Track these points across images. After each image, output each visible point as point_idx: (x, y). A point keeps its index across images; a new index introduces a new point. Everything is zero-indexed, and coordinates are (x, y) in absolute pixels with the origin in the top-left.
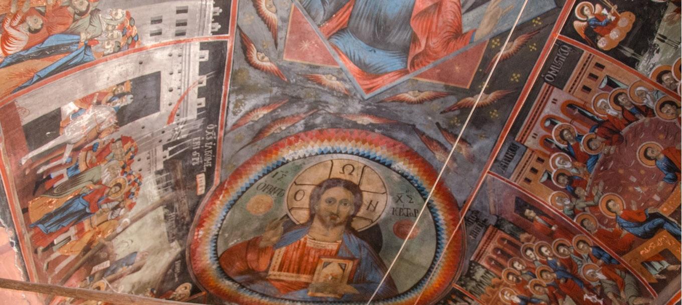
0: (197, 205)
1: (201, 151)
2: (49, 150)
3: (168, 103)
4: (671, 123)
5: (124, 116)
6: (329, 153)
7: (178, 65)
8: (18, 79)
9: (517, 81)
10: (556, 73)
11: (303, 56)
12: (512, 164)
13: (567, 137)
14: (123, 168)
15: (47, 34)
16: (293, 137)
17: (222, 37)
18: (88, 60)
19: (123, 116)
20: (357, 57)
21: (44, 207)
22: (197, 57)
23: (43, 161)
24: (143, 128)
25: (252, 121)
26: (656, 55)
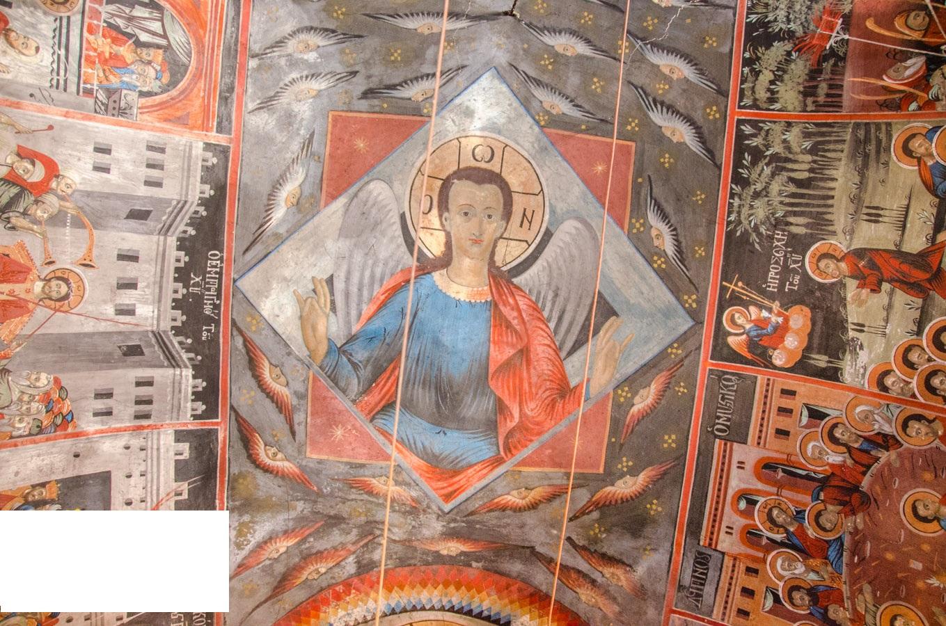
4: (931, 448)
6: (404, 611)
7: (139, 464)
9: (674, 445)
10: (729, 420)
11: (336, 449)
12: (709, 589)
13: (780, 520)
16: (341, 586)
17: (208, 424)
20: (419, 445)
22: (172, 453)
25: (270, 559)
26: (861, 353)
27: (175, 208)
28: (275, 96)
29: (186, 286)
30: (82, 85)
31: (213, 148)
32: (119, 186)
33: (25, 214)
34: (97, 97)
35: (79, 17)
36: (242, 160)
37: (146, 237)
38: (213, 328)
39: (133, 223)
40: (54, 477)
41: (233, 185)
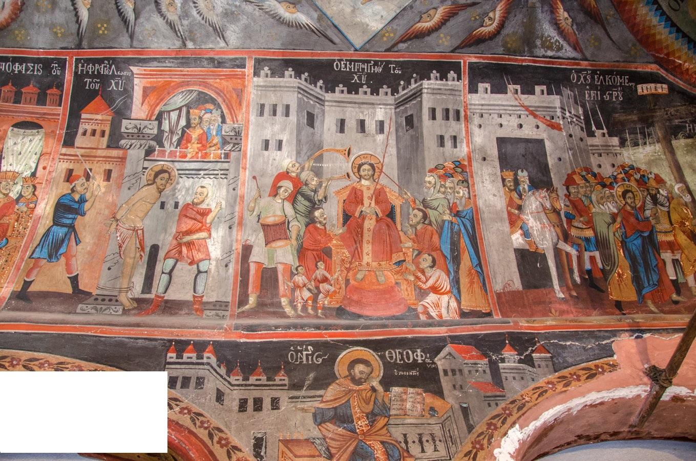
0: (683, 94)
1: (604, 89)
2: (557, 268)
3: (535, 129)
5: (541, 181)
8: (475, 285)
14: (604, 186)
15: (438, 252)
17: (465, 69)
18: (471, 214)
19: (541, 182)
21: (623, 283)
22: (486, 96)
23: (568, 276)
24: (560, 159)
25: (572, 25)
27: (304, 96)
28: (213, 26)
29: (361, 85)
30: (223, 160)
31: (257, 71)
32: (291, 134)
33: (315, 191)
34: (230, 150)
35: (176, 164)
36: (264, 48)
37: (326, 114)
38: (392, 66)
39: (317, 124)
40: (499, 173)
41: (283, 54)
